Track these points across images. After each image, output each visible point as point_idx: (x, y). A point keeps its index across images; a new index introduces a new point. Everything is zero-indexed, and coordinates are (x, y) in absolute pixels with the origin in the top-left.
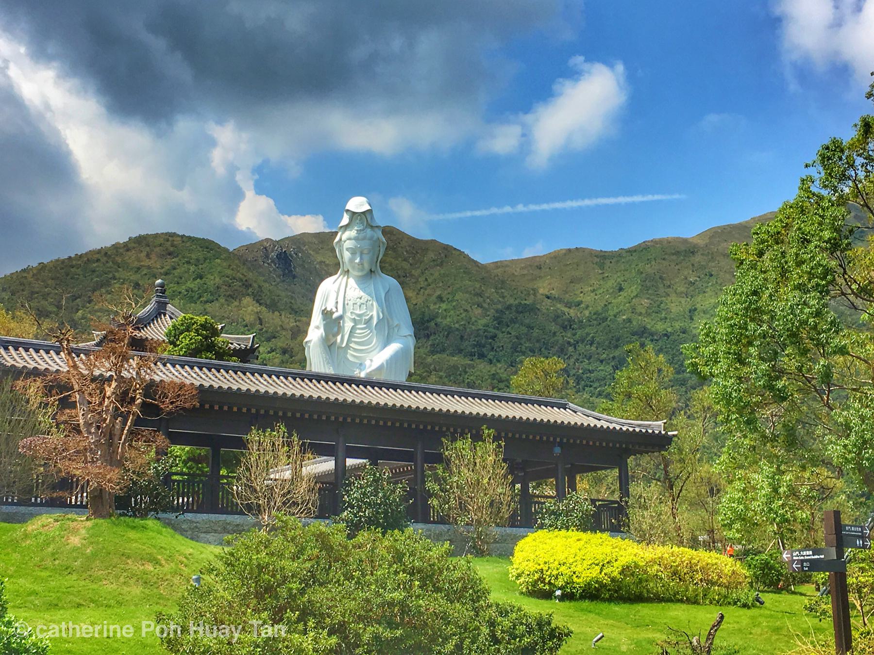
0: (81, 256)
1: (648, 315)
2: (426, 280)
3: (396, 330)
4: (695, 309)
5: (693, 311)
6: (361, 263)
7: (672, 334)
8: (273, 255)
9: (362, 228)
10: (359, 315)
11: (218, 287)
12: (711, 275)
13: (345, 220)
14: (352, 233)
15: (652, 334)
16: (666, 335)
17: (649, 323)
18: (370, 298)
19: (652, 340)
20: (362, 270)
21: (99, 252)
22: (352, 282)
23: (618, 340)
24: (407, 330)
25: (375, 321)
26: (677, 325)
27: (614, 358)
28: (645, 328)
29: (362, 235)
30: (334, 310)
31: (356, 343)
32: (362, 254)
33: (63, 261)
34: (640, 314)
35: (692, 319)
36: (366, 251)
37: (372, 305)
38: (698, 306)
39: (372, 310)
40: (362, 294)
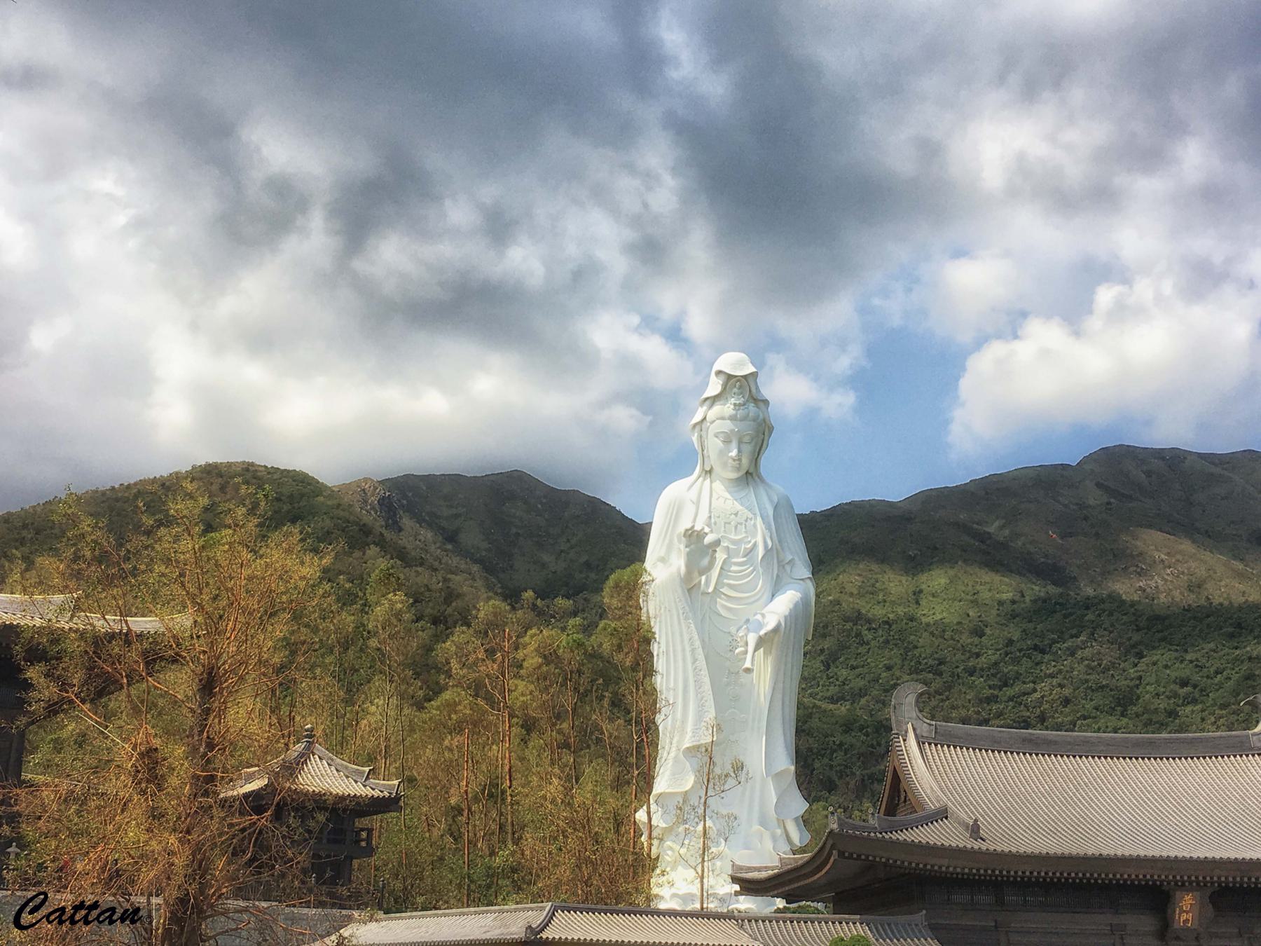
0: (129, 487)
1: (860, 595)
2: (568, 541)
3: (788, 568)
4: (921, 591)
5: (918, 593)
6: (739, 459)
7: (895, 621)
8: (374, 500)
9: (741, 401)
10: (734, 542)
11: (328, 532)
12: (936, 549)
13: (714, 387)
14: (727, 408)
15: (869, 621)
16: (887, 623)
17: (864, 606)
18: (750, 515)
19: (869, 629)
20: (738, 469)
21: (154, 480)
22: (718, 486)
23: (826, 627)
24: (804, 571)
25: (761, 551)
26: (900, 610)
27: (822, 651)
28: (859, 613)
29: (741, 413)
30: (707, 530)
31: (730, 586)
32: (740, 442)
33: (104, 493)
34: (851, 594)
35: (917, 603)
36: (747, 439)
37: (755, 526)
38: (924, 587)
39: (754, 535)
40: (738, 507)
